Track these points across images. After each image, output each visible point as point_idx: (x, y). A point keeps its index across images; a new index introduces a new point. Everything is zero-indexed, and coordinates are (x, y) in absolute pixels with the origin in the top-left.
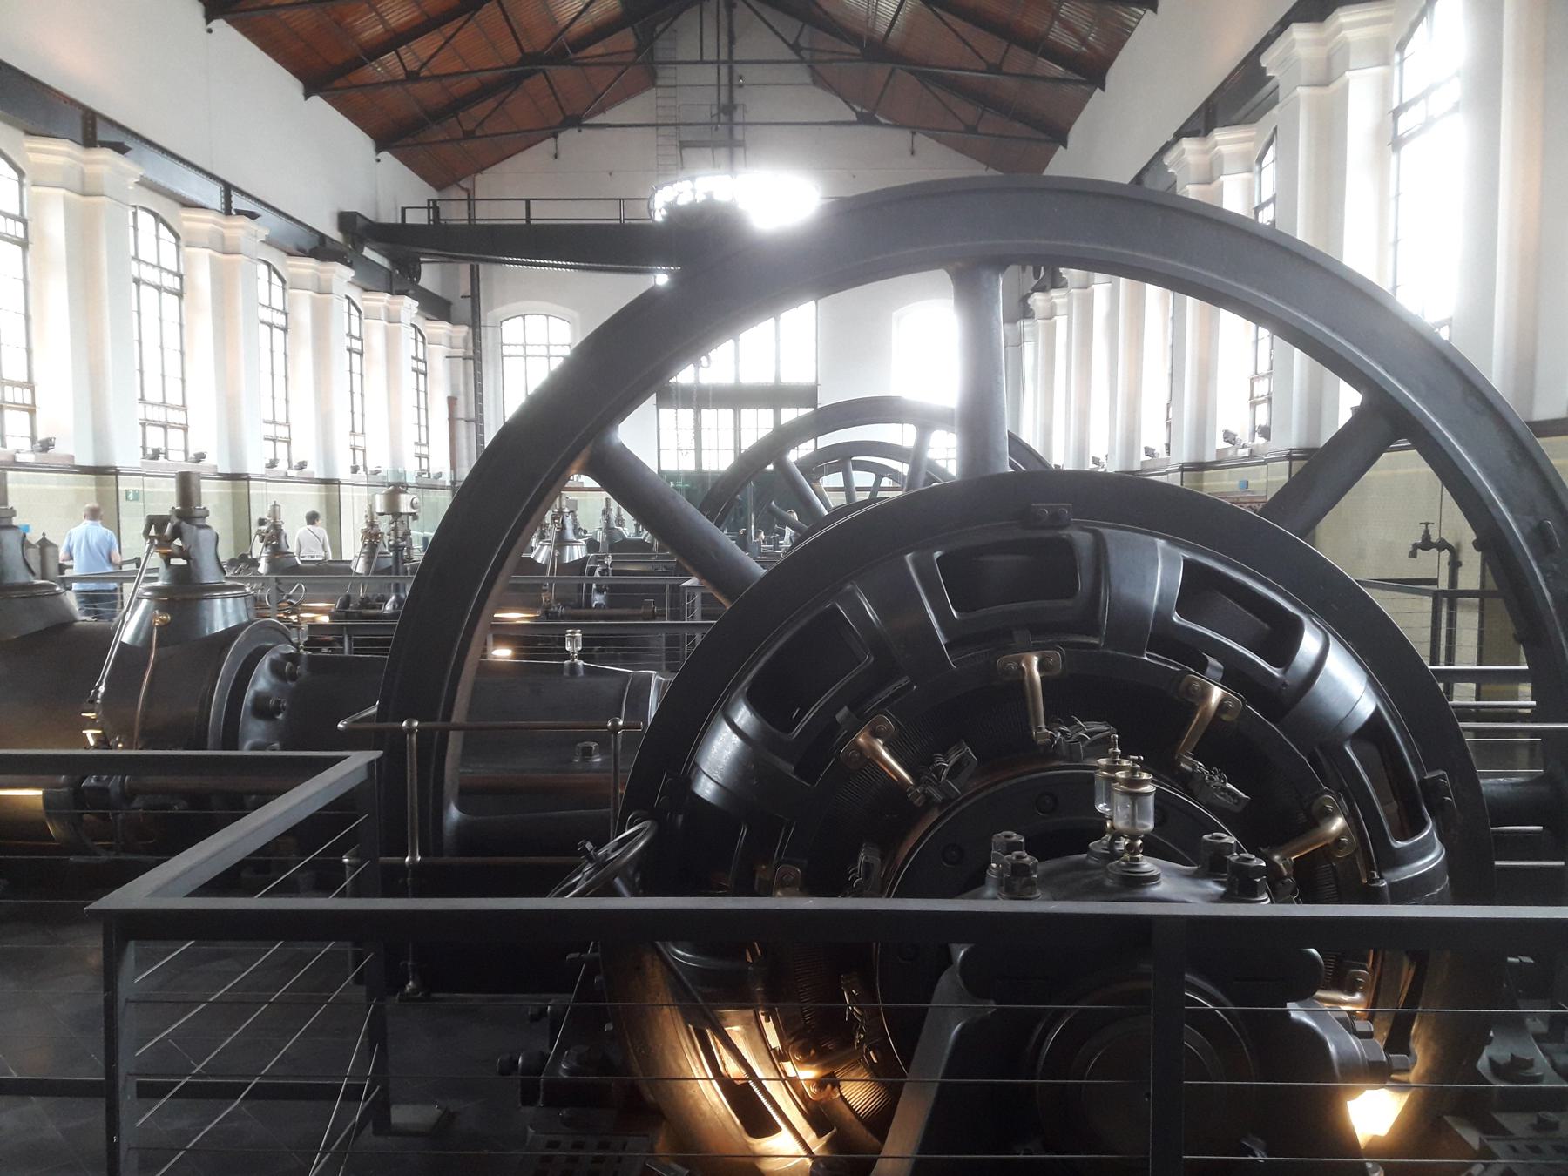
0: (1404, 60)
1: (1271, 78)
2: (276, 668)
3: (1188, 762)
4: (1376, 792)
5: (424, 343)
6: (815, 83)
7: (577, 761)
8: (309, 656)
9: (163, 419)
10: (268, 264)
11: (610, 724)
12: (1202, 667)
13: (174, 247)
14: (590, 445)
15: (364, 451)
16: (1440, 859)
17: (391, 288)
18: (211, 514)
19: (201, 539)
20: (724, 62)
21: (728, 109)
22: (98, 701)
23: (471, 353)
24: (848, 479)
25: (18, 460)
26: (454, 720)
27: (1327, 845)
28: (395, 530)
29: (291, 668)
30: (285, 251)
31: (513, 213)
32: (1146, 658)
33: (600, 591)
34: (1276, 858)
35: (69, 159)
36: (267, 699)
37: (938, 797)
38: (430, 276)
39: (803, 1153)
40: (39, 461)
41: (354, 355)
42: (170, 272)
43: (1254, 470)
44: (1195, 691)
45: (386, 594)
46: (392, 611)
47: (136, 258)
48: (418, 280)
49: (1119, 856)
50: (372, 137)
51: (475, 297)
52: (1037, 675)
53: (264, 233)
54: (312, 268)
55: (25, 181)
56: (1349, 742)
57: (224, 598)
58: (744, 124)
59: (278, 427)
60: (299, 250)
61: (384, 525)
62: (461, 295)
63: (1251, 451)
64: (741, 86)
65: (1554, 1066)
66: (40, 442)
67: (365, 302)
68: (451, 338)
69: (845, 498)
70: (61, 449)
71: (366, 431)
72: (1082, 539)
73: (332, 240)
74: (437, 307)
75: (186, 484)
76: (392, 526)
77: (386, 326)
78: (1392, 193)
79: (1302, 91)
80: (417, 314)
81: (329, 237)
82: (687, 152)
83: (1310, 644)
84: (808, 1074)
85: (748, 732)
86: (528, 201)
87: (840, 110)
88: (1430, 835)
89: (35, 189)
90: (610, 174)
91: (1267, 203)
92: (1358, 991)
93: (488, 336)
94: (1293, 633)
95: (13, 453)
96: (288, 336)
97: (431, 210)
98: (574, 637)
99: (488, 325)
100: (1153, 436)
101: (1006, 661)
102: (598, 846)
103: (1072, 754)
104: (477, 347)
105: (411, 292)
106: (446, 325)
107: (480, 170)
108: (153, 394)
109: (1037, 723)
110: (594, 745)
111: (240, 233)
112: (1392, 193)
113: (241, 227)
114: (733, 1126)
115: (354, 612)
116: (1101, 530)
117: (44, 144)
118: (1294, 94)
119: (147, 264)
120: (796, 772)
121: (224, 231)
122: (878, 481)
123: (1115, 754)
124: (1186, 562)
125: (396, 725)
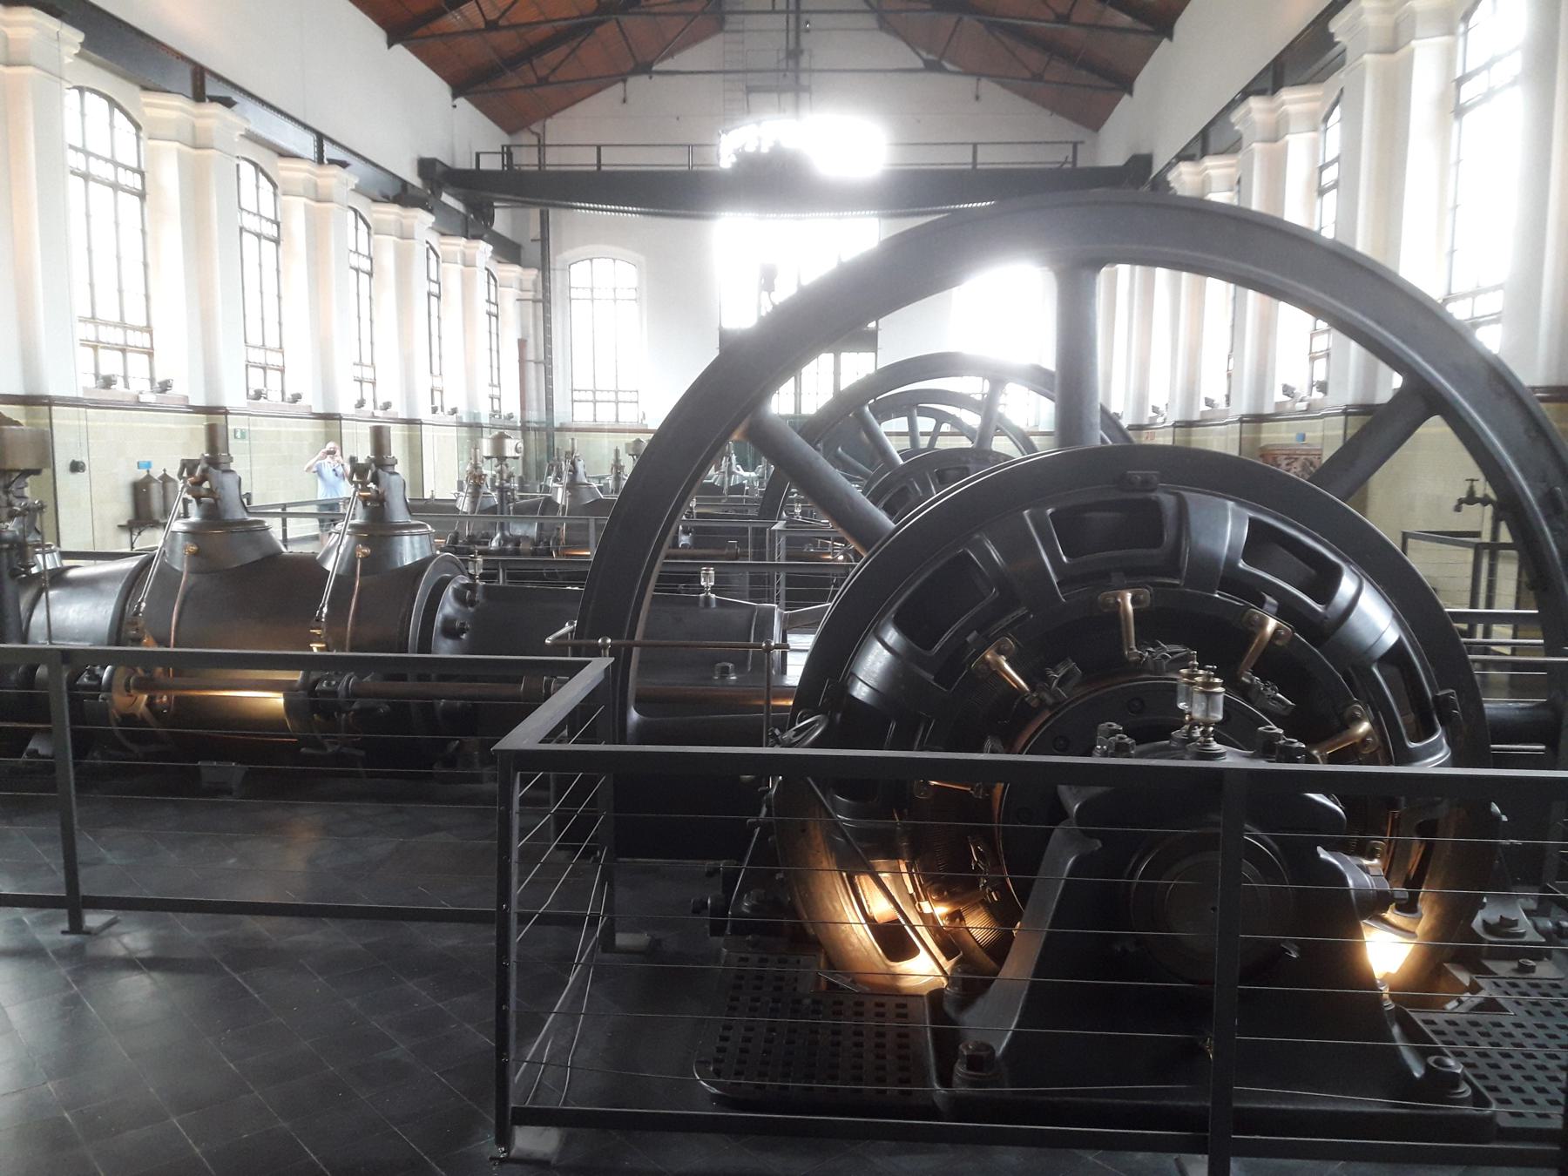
0: (1468, 30)
1: (1338, 43)
2: (459, 596)
3: (1247, 677)
4: (1397, 704)
5: (496, 286)
6: (881, 28)
7: (716, 678)
8: (484, 586)
9: (263, 362)
10: (356, 211)
11: (764, 645)
12: (1261, 603)
13: (272, 196)
14: (750, 416)
15: (442, 392)
16: (1448, 756)
17: (467, 234)
18: (399, 462)
19: (393, 485)
20: (792, 12)
21: (794, 53)
22: (323, 620)
23: (540, 297)
24: (912, 424)
25: (142, 401)
26: (636, 639)
27: (1355, 743)
28: (501, 472)
29: (470, 596)
30: (370, 198)
31: (584, 160)
32: (1217, 596)
33: (686, 532)
34: (1315, 752)
35: (182, 114)
36: (454, 621)
37: (1050, 700)
39: (939, 973)
40: (159, 402)
41: (432, 298)
42: (268, 220)
44: (1255, 622)
45: (490, 532)
46: (499, 548)
47: (356, 252)
49: (1195, 740)
51: (544, 240)
52: (1130, 607)
53: (354, 181)
54: (397, 214)
55: (142, 135)
56: (1376, 664)
57: (412, 535)
58: (812, 71)
59: (364, 368)
60: (384, 197)
61: (489, 470)
62: (532, 238)
63: (1309, 405)
64: (808, 31)
65: (1536, 927)
66: (160, 383)
67: (442, 247)
68: (521, 281)
69: (908, 443)
70: (178, 389)
71: (443, 373)
72: (1167, 501)
73: (413, 186)
74: (509, 251)
75: (379, 438)
76: (499, 468)
77: (462, 273)
78: (1453, 158)
79: (1368, 58)
80: (491, 257)
81: (411, 184)
82: (754, 97)
83: (1347, 586)
84: (941, 910)
85: (897, 649)
86: (599, 148)
87: (903, 55)
88: (1439, 738)
89: (152, 143)
90: (678, 119)
91: (1332, 162)
92: (1376, 857)
93: (556, 277)
94: (1334, 576)
95: (137, 393)
97: (505, 156)
98: (708, 574)
100: (1213, 387)
101: (1105, 596)
102: (783, 731)
103: (1157, 669)
104: (546, 289)
105: (486, 236)
106: (517, 269)
107: (550, 115)
108: (255, 339)
109: (1129, 644)
110: (731, 665)
111: (334, 181)
112: (1453, 158)
113: (335, 176)
114: (876, 955)
115: (463, 548)
116: (1182, 492)
118: (1360, 61)
119: (249, 212)
120: (935, 680)
121: (319, 181)
122: (938, 426)
123: (1194, 666)
124: (1250, 519)
125: (615, 642)
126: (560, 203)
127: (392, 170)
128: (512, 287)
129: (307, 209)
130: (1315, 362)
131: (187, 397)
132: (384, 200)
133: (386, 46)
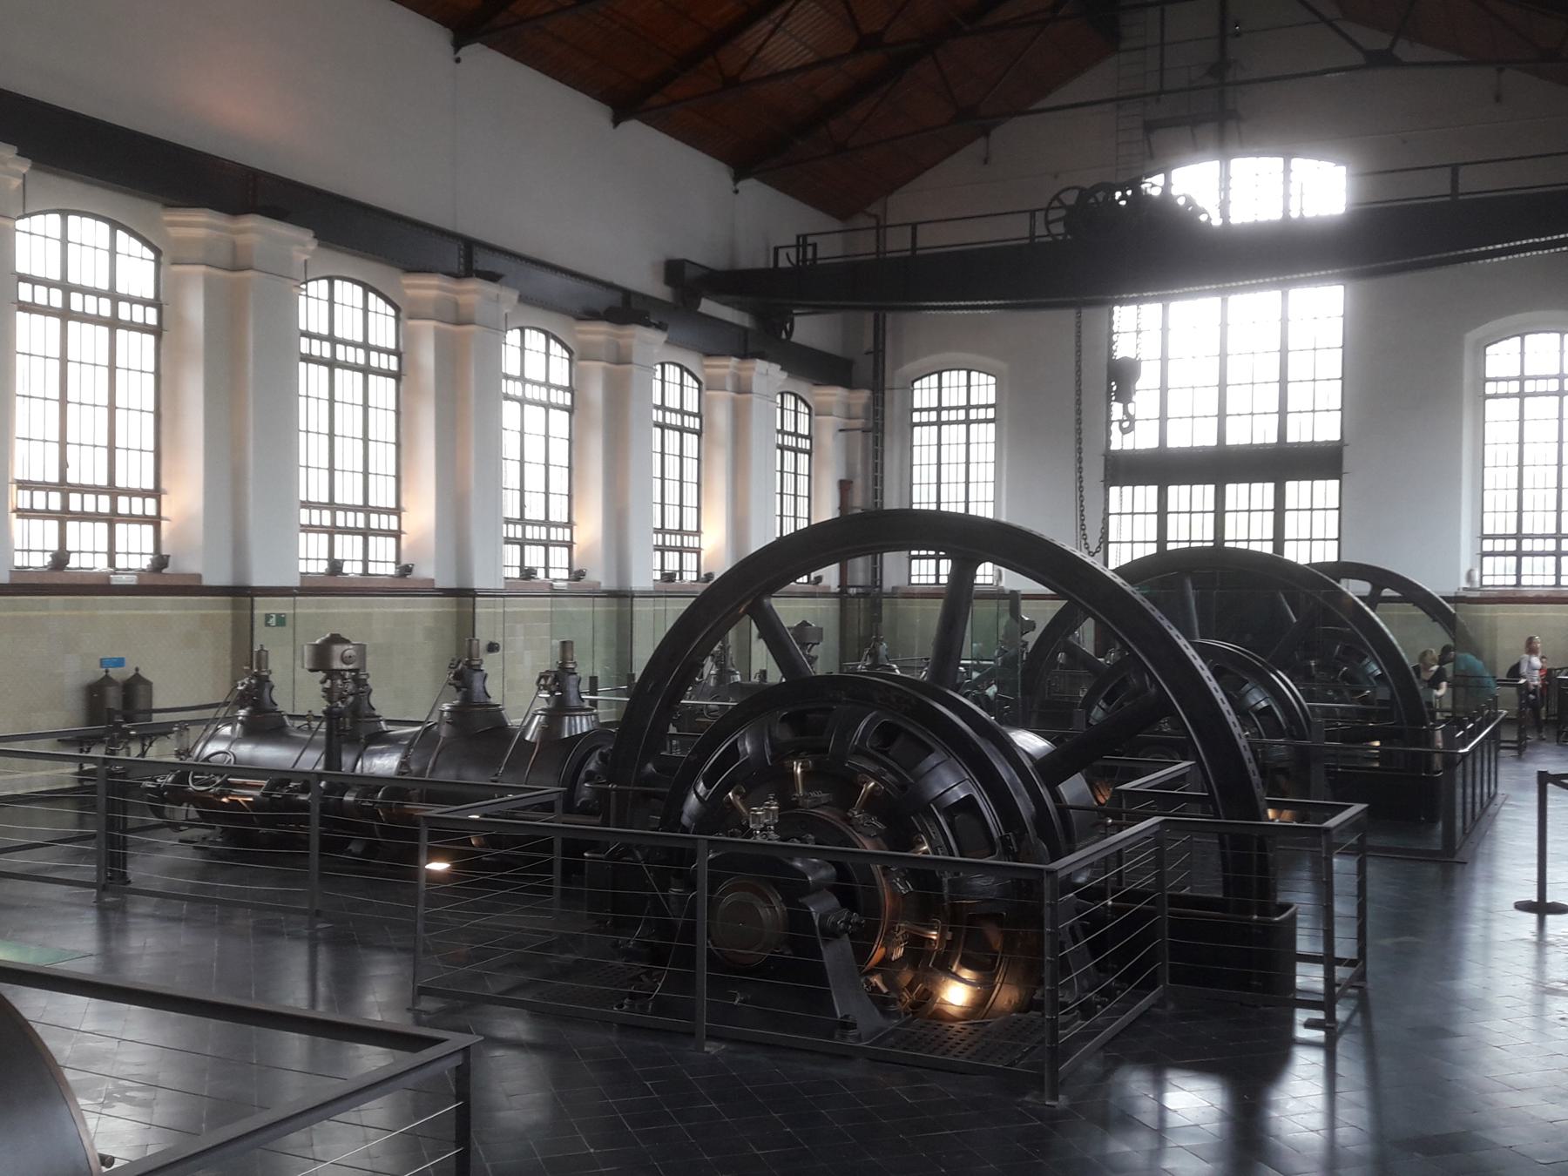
38: (808, 330)
43: (47, 601)
48: (789, 334)
50: (726, 163)
51: (878, 353)
64: (1238, 35)
68: (848, 406)
77: (734, 401)
93: (893, 399)
96: (574, 418)
99: (896, 386)
107: (891, 192)
113: (475, 291)
117: (180, 216)
121: (457, 297)
126: (899, 304)
127: (606, 278)
128: (831, 415)
129: (440, 337)
130: (1558, 372)
131: (822, 629)
132: (587, 317)
133: (612, 125)
